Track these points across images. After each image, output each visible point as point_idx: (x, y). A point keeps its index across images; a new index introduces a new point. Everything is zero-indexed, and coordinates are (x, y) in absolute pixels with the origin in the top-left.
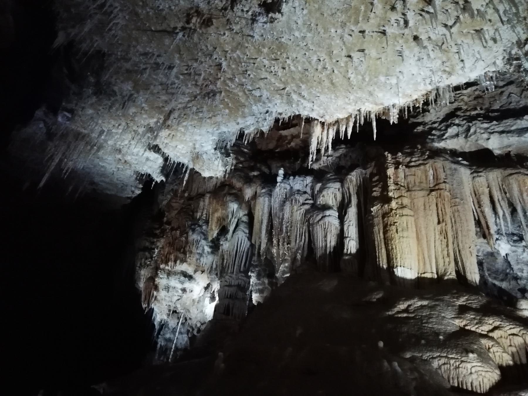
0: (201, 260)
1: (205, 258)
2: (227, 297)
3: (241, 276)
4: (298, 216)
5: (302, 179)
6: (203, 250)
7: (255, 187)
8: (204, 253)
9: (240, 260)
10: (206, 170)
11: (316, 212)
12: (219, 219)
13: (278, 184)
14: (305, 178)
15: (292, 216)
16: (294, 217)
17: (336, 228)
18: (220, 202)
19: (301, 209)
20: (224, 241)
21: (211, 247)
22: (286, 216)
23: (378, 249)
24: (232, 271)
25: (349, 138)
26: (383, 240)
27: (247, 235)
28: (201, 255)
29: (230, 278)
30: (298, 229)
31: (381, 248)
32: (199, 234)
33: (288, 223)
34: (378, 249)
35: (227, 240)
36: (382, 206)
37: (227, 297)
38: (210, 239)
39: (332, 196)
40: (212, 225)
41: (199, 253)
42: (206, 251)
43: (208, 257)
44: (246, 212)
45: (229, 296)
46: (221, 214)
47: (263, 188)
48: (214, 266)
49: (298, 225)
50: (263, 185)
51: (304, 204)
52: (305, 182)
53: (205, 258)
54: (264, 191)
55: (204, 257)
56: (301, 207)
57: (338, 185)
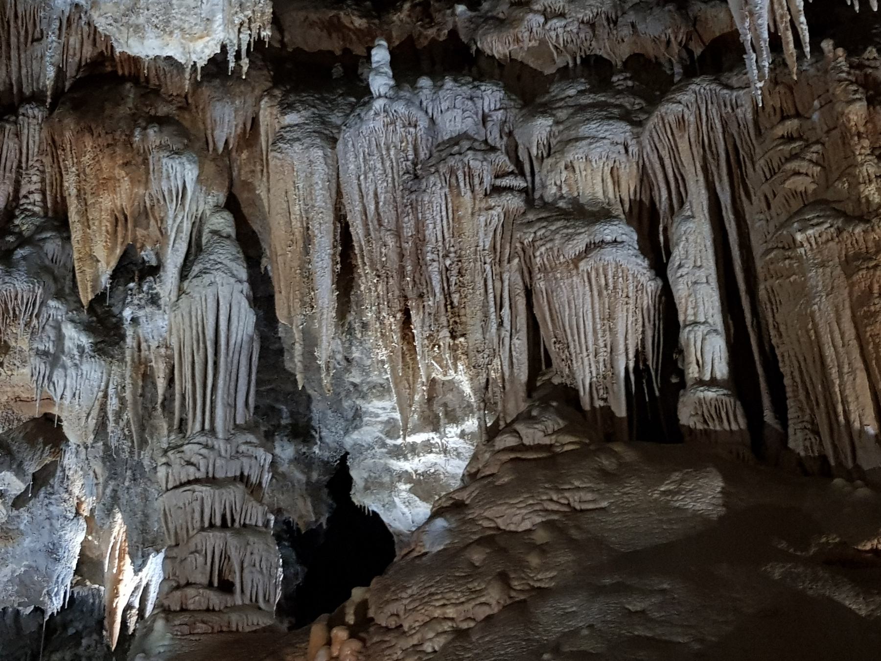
0: (55, 379)
1: (72, 372)
2: (212, 526)
3: (246, 443)
4: (481, 234)
5: (466, 90)
6: (60, 338)
7: (250, 101)
8: (63, 352)
9: (233, 384)
10: (150, 33)
11: (559, 224)
12: (119, 219)
13: (378, 104)
14: (478, 87)
15: (457, 233)
16: (468, 240)
17: (640, 288)
18: (119, 151)
19: (490, 208)
20: (140, 307)
21: (88, 328)
22: (432, 232)
23: (841, 374)
24: (207, 426)
25: (875, 9)
26: (854, 343)
27: (246, 286)
28: (53, 359)
29: (204, 451)
30: (490, 283)
31: (853, 372)
32: (37, 275)
33: (446, 256)
34: (841, 374)
35: (154, 300)
36: (840, 231)
37: (212, 526)
38: (86, 296)
39: (602, 168)
40: (87, 240)
41: (46, 353)
42: (68, 344)
43: (85, 367)
44: (222, 199)
45: (218, 521)
46: (131, 199)
47: (286, 107)
48: (113, 404)
49: (488, 267)
50: (277, 92)
51: (497, 190)
52: (479, 103)
53: (72, 372)
54: (291, 118)
55: (64, 368)
56: (492, 202)
57: (620, 131)
